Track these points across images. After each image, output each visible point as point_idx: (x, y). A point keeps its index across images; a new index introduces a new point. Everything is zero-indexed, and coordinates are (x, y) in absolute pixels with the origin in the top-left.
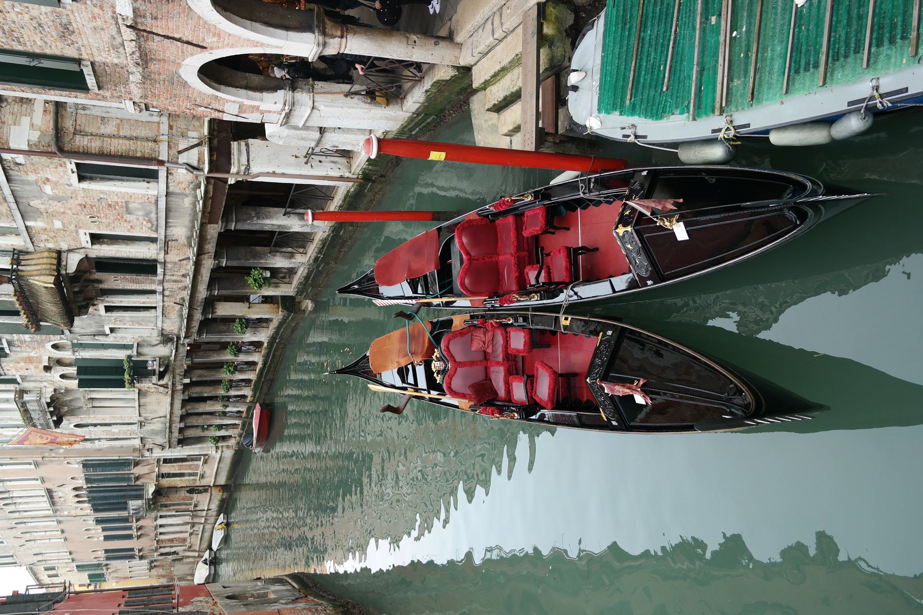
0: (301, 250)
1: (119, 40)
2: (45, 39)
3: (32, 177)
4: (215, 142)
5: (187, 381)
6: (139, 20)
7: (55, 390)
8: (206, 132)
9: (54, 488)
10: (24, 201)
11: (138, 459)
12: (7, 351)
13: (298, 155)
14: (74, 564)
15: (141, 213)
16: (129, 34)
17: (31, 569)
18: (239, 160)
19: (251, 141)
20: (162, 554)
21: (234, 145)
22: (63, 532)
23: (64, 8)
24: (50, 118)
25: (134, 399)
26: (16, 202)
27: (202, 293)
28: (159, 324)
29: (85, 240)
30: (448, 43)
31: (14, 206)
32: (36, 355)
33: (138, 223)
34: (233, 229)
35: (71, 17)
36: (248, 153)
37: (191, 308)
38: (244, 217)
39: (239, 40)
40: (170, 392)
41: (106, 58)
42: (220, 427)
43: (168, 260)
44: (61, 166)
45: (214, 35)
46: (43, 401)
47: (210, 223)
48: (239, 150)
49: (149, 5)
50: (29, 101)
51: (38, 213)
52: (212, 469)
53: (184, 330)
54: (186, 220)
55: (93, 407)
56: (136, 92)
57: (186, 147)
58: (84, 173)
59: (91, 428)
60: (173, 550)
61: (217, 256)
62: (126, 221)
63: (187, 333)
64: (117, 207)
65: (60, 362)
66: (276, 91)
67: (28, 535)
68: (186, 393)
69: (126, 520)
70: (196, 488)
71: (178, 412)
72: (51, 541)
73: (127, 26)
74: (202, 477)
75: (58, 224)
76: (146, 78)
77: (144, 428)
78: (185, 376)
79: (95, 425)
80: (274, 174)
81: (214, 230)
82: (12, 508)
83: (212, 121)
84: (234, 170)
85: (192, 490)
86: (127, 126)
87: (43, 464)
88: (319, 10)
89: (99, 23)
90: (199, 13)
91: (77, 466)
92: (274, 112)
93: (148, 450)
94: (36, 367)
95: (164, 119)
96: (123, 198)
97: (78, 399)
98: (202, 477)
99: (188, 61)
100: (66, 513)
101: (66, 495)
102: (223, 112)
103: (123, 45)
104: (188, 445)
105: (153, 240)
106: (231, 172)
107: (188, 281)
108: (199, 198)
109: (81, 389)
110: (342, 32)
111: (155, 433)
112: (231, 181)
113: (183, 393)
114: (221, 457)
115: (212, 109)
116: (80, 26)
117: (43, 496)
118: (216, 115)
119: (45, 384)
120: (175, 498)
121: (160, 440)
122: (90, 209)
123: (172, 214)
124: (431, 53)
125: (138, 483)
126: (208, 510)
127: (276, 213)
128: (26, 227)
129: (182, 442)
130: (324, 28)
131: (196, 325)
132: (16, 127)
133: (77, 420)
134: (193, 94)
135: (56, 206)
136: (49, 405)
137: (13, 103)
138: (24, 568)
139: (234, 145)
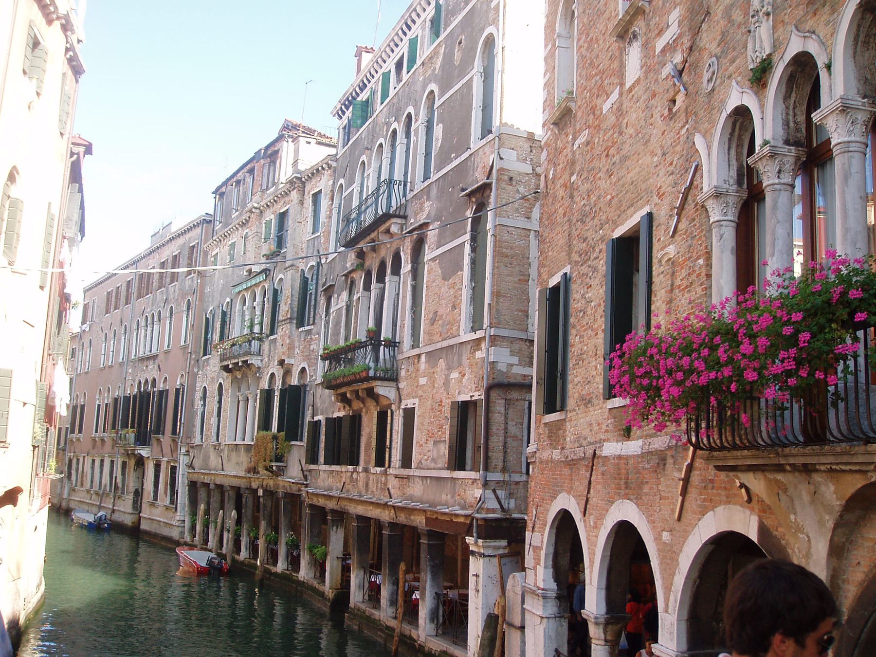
1: (584, 443)
2: (579, 384)
3: (465, 362)
5: (260, 492)
6: (601, 461)
12: (301, 329)
15: (435, 454)
16: (590, 452)
20: (70, 461)
23: (604, 402)
24: (519, 380)
25: (244, 440)
29: (408, 403)
31: (439, 346)
32: (296, 353)
33: (425, 451)
34: (421, 541)
35: (598, 407)
40: (249, 475)
41: (569, 431)
44: (476, 387)
45: (595, 523)
47: (427, 519)
48: (498, 548)
50: (531, 364)
52: (159, 516)
55: (239, 401)
57: (500, 496)
59: (217, 398)
60: (73, 472)
62: (427, 440)
63: (313, 494)
64: (440, 433)
65: (287, 373)
66: (555, 581)
70: (139, 498)
72: (103, 356)
73: (595, 450)
75: (423, 381)
77: (212, 449)
78: (265, 491)
79: (220, 402)
81: (419, 521)
83: (411, 468)
85: (138, 494)
86: (515, 444)
89: (596, 428)
92: (536, 580)
93: (188, 451)
94: (284, 353)
98: (152, 505)
100: (130, 371)
101: (150, 372)
102: (533, 531)
103: (581, 446)
104: (189, 491)
106: (479, 540)
109: (259, 391)
110: (611, 641)
111: (206, 458)
113: (247, 488)
114: (172, 525)
115: (535, 521)
116: (592, 413)
117: (151, 351)
118: (530, 525)
119: (266, 359)
121: (197, 463)
128: (419, 356)
129: (193, 486)
130: (612, 624)
131: (321, 502)
133: (227, 385)
134: (547, 504)
135: (440, 381)
136: (245, 362)
137: (530, 351)
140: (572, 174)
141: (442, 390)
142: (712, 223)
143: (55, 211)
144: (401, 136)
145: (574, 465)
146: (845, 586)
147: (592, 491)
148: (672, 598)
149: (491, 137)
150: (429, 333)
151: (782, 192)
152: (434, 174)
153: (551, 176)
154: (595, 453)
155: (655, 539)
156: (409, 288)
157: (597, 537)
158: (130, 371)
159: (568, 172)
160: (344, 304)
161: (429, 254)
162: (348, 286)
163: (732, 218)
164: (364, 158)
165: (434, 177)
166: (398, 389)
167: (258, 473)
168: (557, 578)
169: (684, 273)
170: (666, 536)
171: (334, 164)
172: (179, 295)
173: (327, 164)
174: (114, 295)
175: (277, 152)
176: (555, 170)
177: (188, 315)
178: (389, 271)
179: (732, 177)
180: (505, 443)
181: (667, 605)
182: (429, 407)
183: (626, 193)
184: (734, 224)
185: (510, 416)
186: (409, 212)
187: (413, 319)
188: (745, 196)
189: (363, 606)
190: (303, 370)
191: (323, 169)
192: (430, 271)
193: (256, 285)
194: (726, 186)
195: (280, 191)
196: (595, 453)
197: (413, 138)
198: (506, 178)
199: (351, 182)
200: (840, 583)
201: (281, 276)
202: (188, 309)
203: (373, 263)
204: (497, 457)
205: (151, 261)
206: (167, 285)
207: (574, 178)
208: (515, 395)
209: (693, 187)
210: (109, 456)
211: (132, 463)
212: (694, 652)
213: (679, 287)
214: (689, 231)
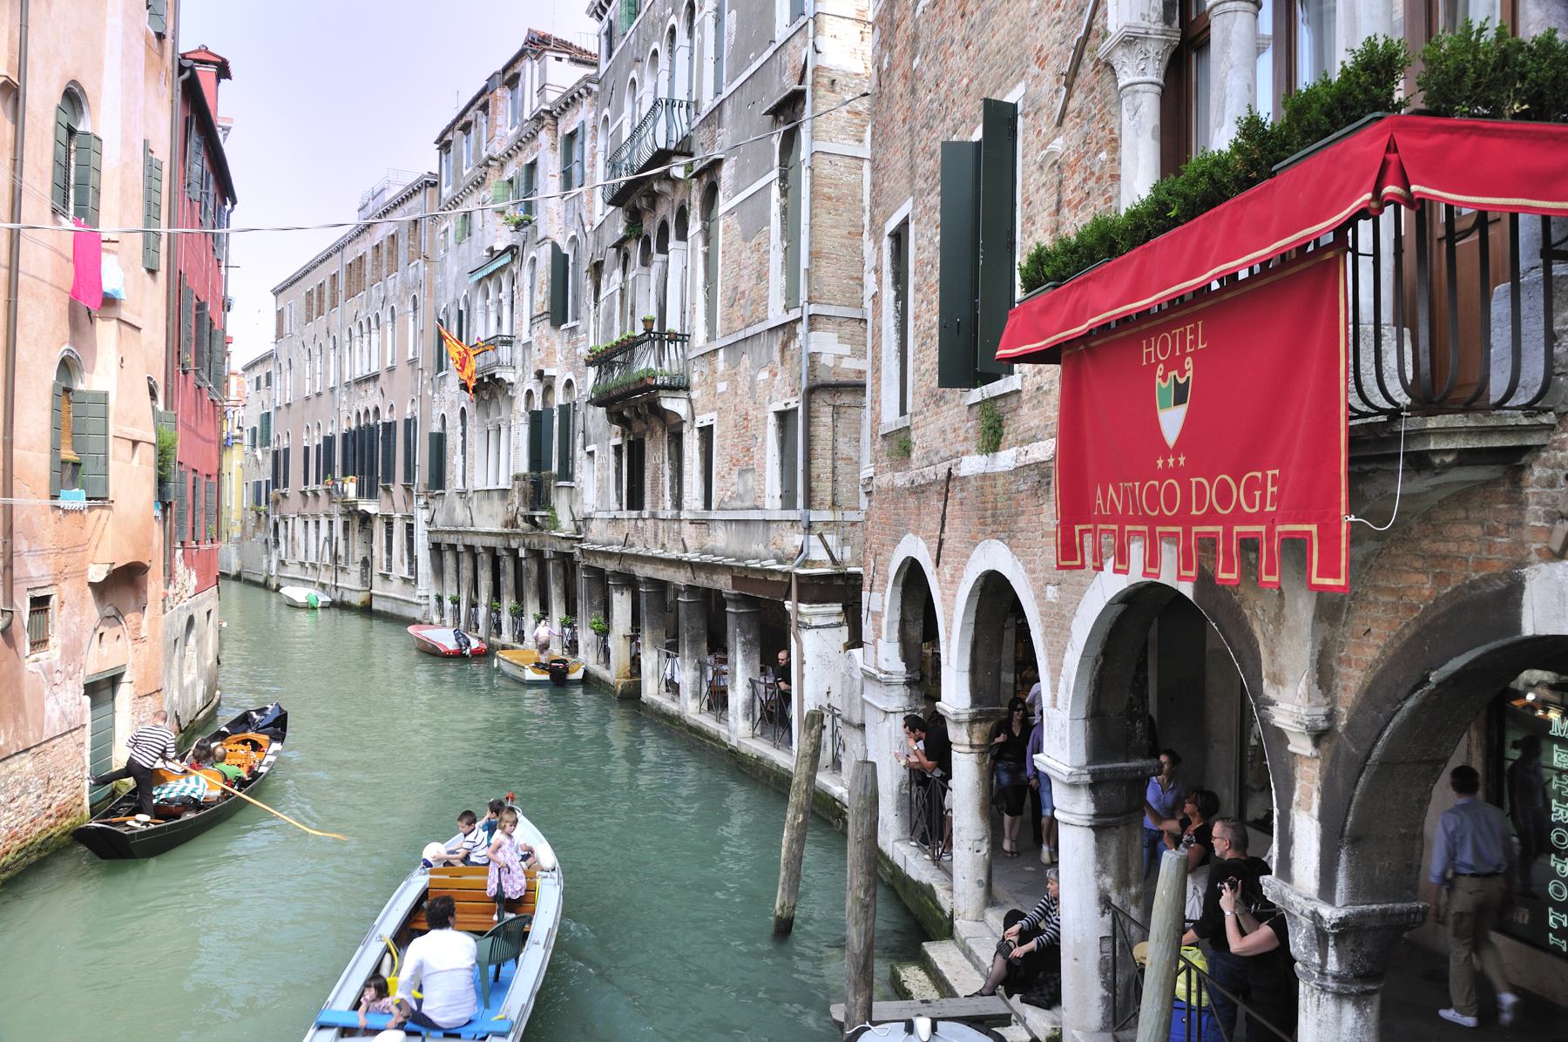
0: (705, 706)
1: (936, 460)
4: (840, 582)
5: (522, 553)
6: (957, 484)
7: (512, 384)
8: (849, 570)
9: (379, 384)
10: (748, 347)
11: (414, 490)
12: (563, 327)
13: (831, 695)
14: (272, 410)
15: (741, 488)
16: (942, 470)
17: (271, 356)
18: (817, 614)
19: (845, 629)
20: (276, 525)
21: (838, 608)
22: (319, 395)
24: (852, 378)
26: (746, 339)
27: (643, 571)
28: (599, 515)
29: (703, 419)
30: (982, 900)
31: (741, 336)
35: (953, 404)
36: (828, 626)
37: (621, 556)
38: (744, 624)
39: (950, 608)
40: (506, 530)
42: (456, 602)
43: (683, 524)
45: (952, 576)
46: (497, 370)
47: (734, 578)
48: (830, 615)
49: (973, 495)
51: (734, 364)
53: (591, 547)
54: (735, 547)
56: (884, 480)
57: (829, 544)
58: (785, 418)
59: (460, 429)
60: (281, 540)
61: (691, 589)
63: (588, 551)
66: (904, 660)
67: (318, 352)
68: (504, 553)
69: (329, 469)
71: (478, 542)
74: (386, 577)
75: (722, 387)
76: (897, 494)
77: (457, 498)
78: (528, 550)
79: (464, 434)
80: (802, 663)
81: (723, 583)
82: (356, 332)
84: (803, 607)
85: (366, 563)
86: (849, 469)
87: (413, 370)
88: (1003, 713)
89: (950, 436)
90: (973, 557)
91: (409, 411)
93: (426, 503)
94: (542, 361)
95: (862, 517)
96: (759, 466)
97: (500, 413)
99: (922, 544)
101: (370, 398)
105: (708, 505)
107: (657, 552)
108: (764, 563)
110: (979, 746)
111: (451, 512)
112: (788, 605)
118: (867, 582)
119: (520, 372)
120: (357, 540)
121: (440, 519)
122: (744, 424)
123: (742, 527)
124: (966, 876)
125: (381, 491)
126: (337, 588)
127: (753, 669)
128: (716, 351)
129: (436, 549)
130: (980, 721)
131: (599, 563)
132: (836, 340)
133: (470, 410)
134: (888, 551)
135: (744, 386)
136: (492, 376)
138: (273, 346)
139: (838, 608)
140: (913, 57)
141: (746, 399)
142: (1122, 89)
143: (162, 152)
144: (681, 34)
145: (923, 492)
146: (1343, 670)
147: (946, 529)
148: (1062, 686)
149: (802, 20)
150: (728, 319)
151: (1240, 14)
152: (728, 86)
153: (885, 66)
154: (950, 473)
155: (1037, 597)
156: (700, 257)
157: (954, 596)
158: (344, 399)
159: (907, 57)
160: (617, 287)
161: (724, 204)
162: (621, 261)
163: (1154, 79)
164: (634, 74)
165: (726, 92)
166: (690, 400)
167: (518, 527)
168: (906, 657)
169: (1078, 178)
170: (1052, 592)
171: (595, 88)
172: (401, 290)
173: (587, 88)
174: (315, 295)
175: (517, 77)
176: (891, 56)
177: (415, 317)
178: (672, 234)
179: (1155, 9)
180: (834, 468)
181: (1055, 698)
182: (732, 423)
183: (991, 69)
184: (1158, 89)
185: (840, 429)
186: (695, 147)
187: (707, 301)
188: (1176, 38)
189: (659, 699)
190: (569, 384)
191: (581, 95)
192: (726, 225)
193: (501, 269)
194: (1145, 24)
195: (524, 133)
196: (950, 473)
197: (697, 35)
198: (826, 81)
199: (619, 111)
200: (1334, 664)
201: (533, 254)
202: (415, 309)
203: (650, 227)
204: (823, 489)
205: (359, 246)
206: (384, 277)
207: (917, 62)
208: (846, 399)
209: (1091, 36)
210: (326, 515)
211: (356, 523)
212: (1097, 767)
213: (1069, 202)
214: (1085, 110)
